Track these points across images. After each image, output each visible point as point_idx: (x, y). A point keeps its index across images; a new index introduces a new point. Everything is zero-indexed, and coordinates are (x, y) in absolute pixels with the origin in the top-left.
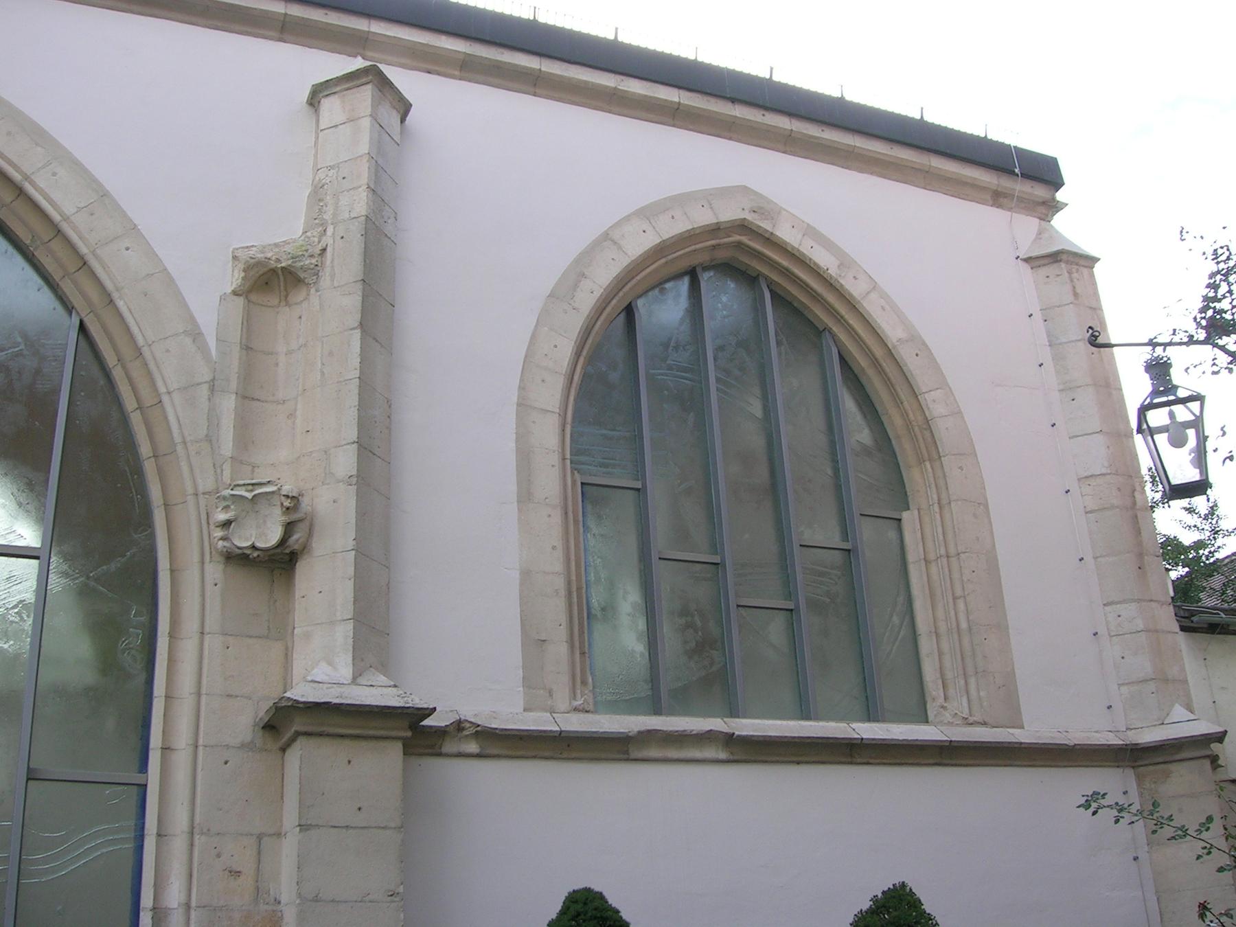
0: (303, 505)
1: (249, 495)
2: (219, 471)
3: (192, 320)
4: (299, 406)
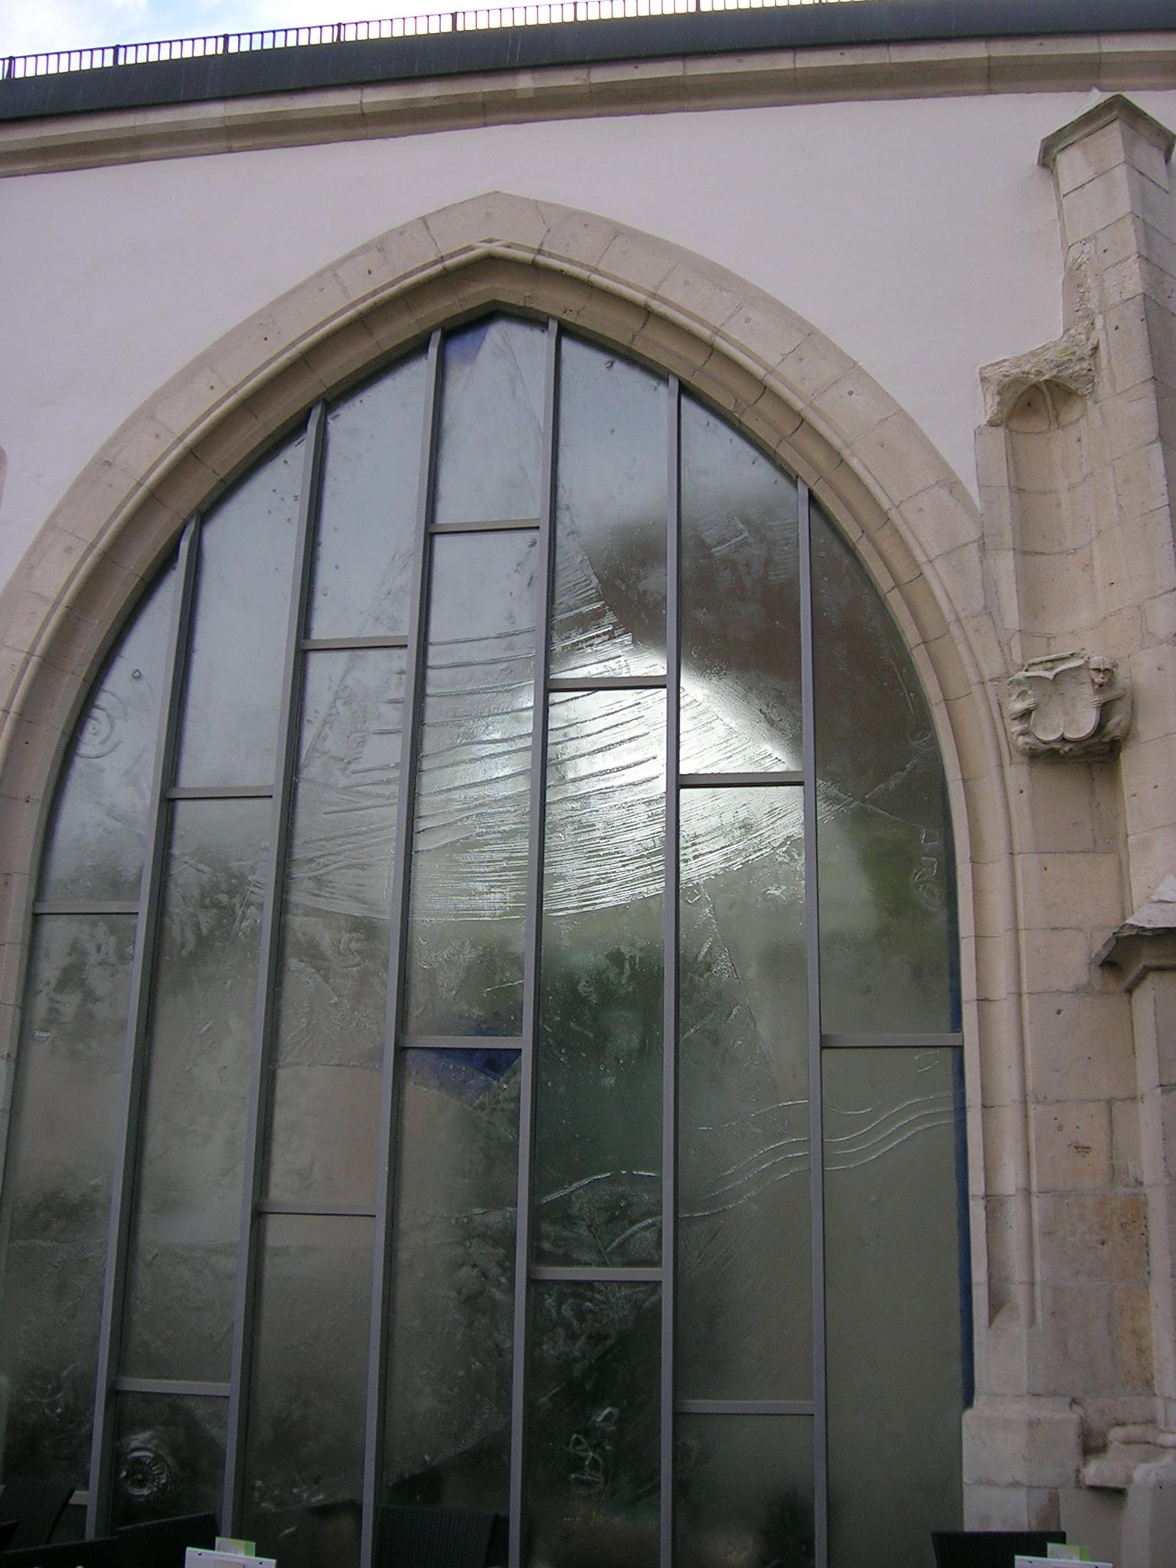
0: (1119, 678)
1: (1050, 675)
2: (1006, 650)
3: (944, 466)
4: (1096, 554)
